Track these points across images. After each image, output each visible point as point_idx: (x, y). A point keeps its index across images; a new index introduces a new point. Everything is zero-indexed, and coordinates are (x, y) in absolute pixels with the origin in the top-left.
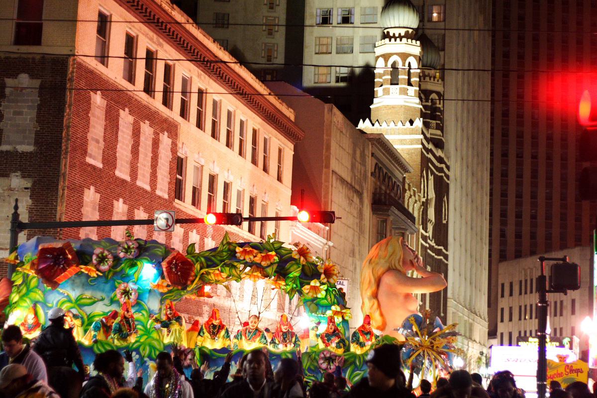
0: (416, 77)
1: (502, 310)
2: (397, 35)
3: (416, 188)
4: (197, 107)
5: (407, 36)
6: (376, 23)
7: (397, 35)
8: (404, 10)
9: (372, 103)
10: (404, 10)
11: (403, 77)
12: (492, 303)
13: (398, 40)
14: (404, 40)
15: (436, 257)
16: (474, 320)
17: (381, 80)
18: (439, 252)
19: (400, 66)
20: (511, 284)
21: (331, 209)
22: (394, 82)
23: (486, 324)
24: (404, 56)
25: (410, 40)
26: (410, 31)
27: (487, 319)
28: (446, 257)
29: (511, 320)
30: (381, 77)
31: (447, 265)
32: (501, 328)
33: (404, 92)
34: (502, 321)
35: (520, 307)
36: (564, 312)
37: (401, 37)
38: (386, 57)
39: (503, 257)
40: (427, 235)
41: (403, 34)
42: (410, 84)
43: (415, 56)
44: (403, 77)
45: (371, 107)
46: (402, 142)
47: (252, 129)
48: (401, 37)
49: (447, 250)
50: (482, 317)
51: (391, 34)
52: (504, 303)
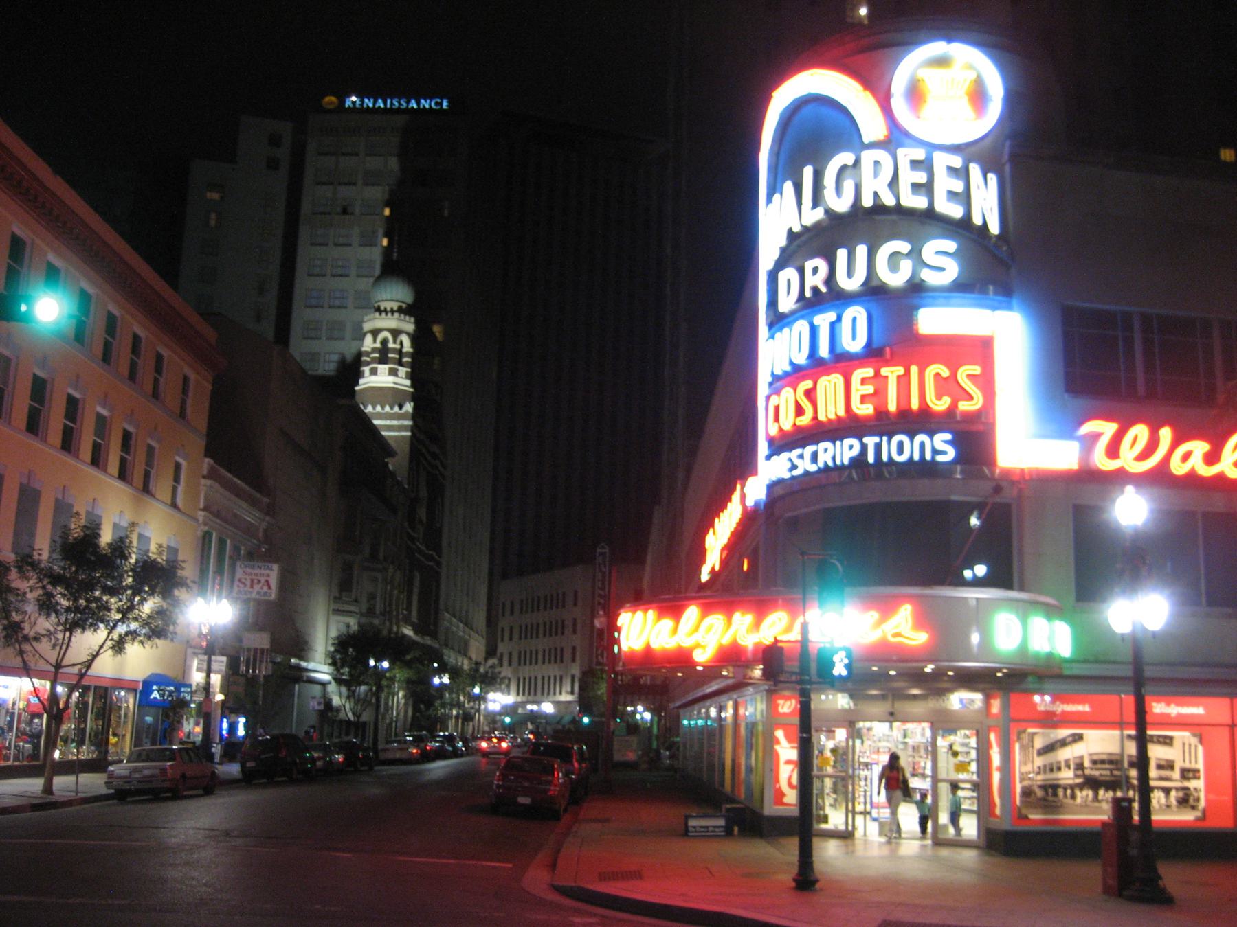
0: (409, 357)
1: (503, 630)
2: (388, 309)
3: (447, 750)
4: (29, 402)
5: (400, 310)
6: (350, 245)
7: (388, 309)
8: (313, 650)
9: (357, 384)
10: (313, 650)
11: (56, 420)
12: (491, 622)
13: (390, 314)
14: (396, 315)
15: (426, 562)
16: (470, 636)
17: (368, 359)
18: (431, 558)
19: (391, 345)
20: (512, 603)
21: (216, 661)
22: (383, 360)
23: (483, 641)
24: (395, 333)
25: (402, 316)
26: (404, 306)
27: (485, 636)
28: (439, 564)
29: (511, 639)
30: (368, 356)
31: (438, 573)
32: (502, 648)
33: (393, 372)
34: (502, 640)
35: (521, 627)
36: (566, 632)
37: (392, 311)
38: (375, 333)
39: (505, 576)
40: (416, 535)
41: (395, 308)
42: (401, 364)
43: (408, 334)
44: (56, 420)
45: (357, 388)
46: (390, 428)
47: (814, 210)
48: (392, 311)
49: (440, 557)
50: (480, 633)
51: (382, 308)
52: (504, 623)
